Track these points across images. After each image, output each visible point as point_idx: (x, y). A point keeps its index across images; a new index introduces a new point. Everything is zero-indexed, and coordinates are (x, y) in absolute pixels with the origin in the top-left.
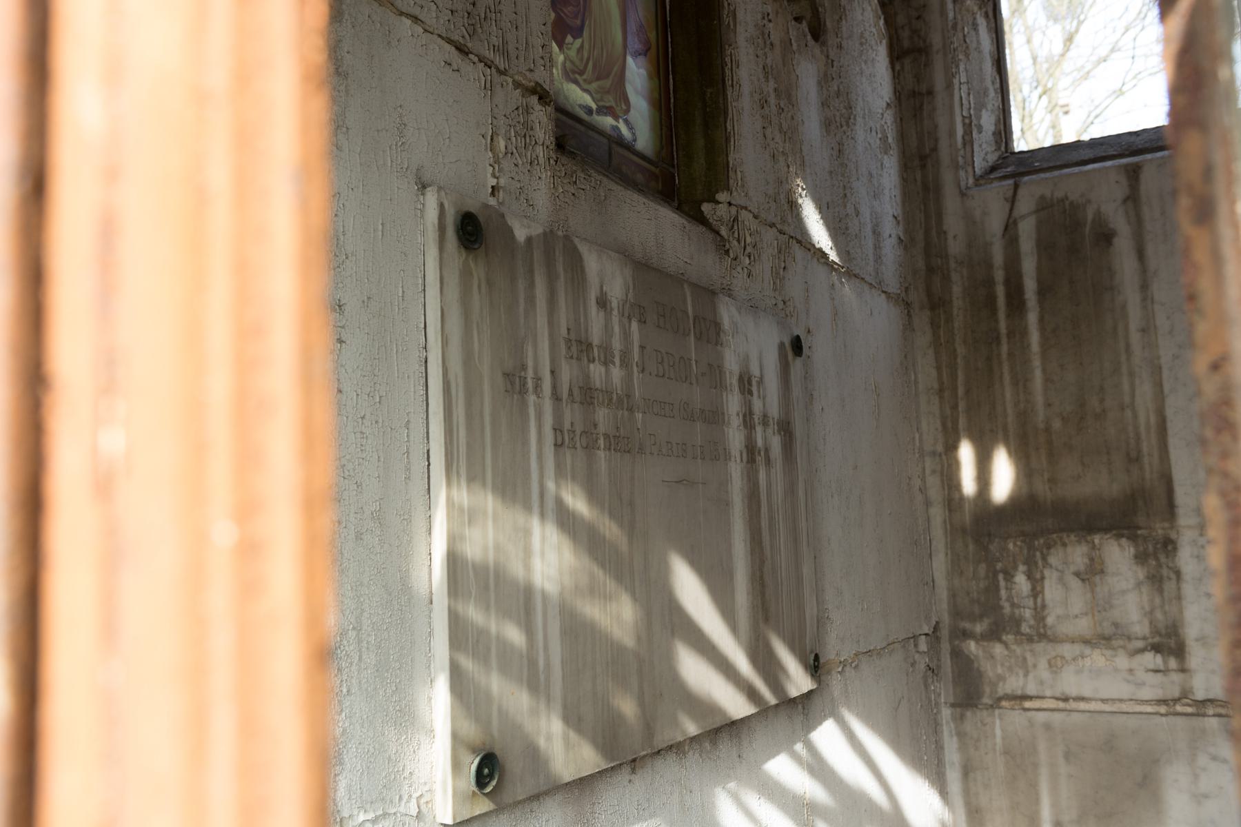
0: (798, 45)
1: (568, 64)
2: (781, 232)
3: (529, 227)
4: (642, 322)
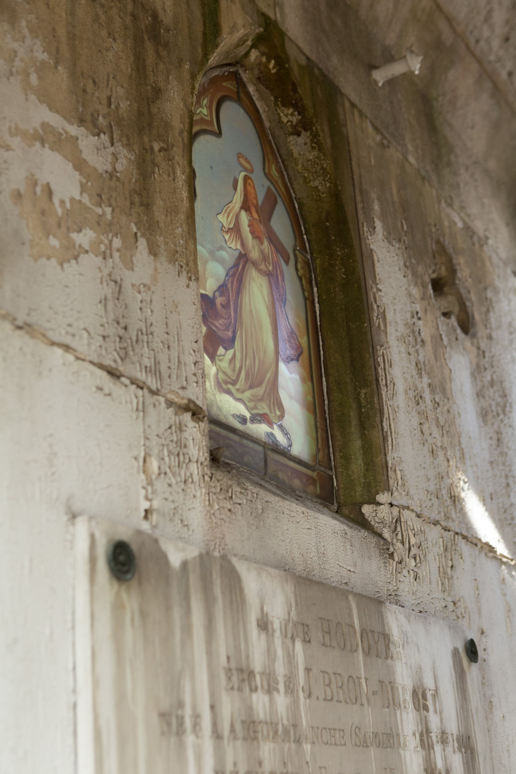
0: (449, 340)
1: (221, 376)
2: (446, 529)
3: (184, 550)
4: (307, 641)
